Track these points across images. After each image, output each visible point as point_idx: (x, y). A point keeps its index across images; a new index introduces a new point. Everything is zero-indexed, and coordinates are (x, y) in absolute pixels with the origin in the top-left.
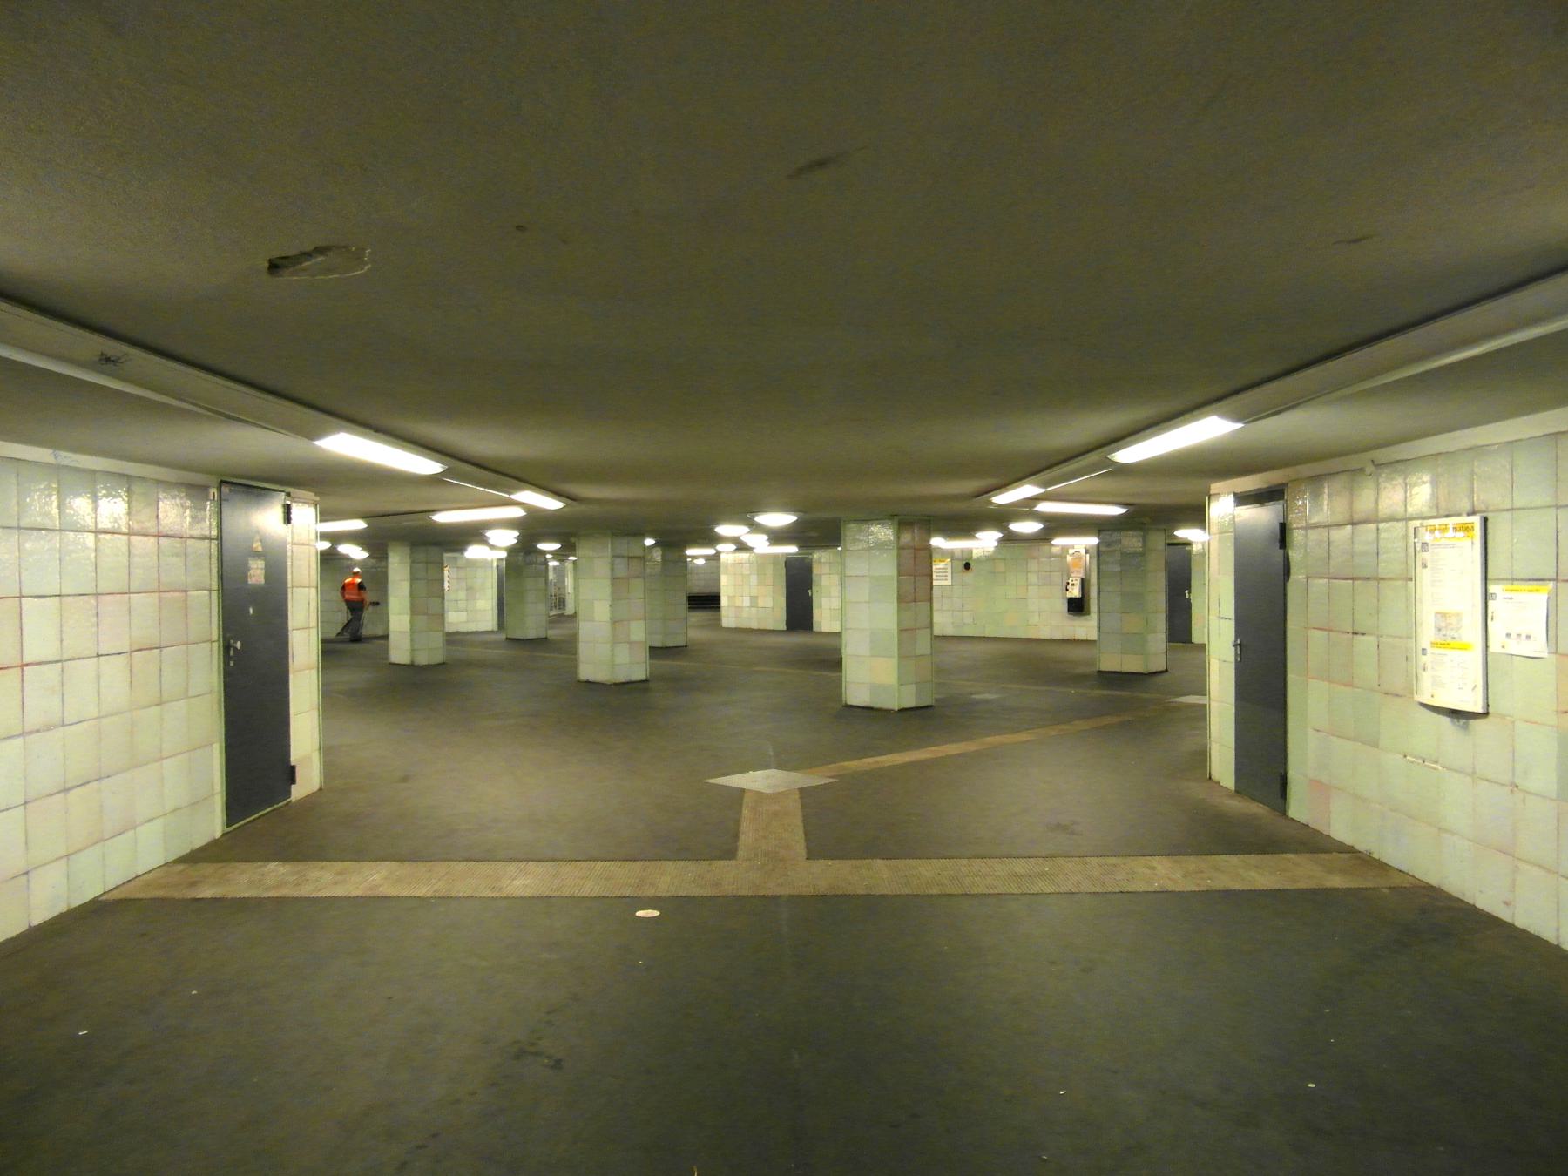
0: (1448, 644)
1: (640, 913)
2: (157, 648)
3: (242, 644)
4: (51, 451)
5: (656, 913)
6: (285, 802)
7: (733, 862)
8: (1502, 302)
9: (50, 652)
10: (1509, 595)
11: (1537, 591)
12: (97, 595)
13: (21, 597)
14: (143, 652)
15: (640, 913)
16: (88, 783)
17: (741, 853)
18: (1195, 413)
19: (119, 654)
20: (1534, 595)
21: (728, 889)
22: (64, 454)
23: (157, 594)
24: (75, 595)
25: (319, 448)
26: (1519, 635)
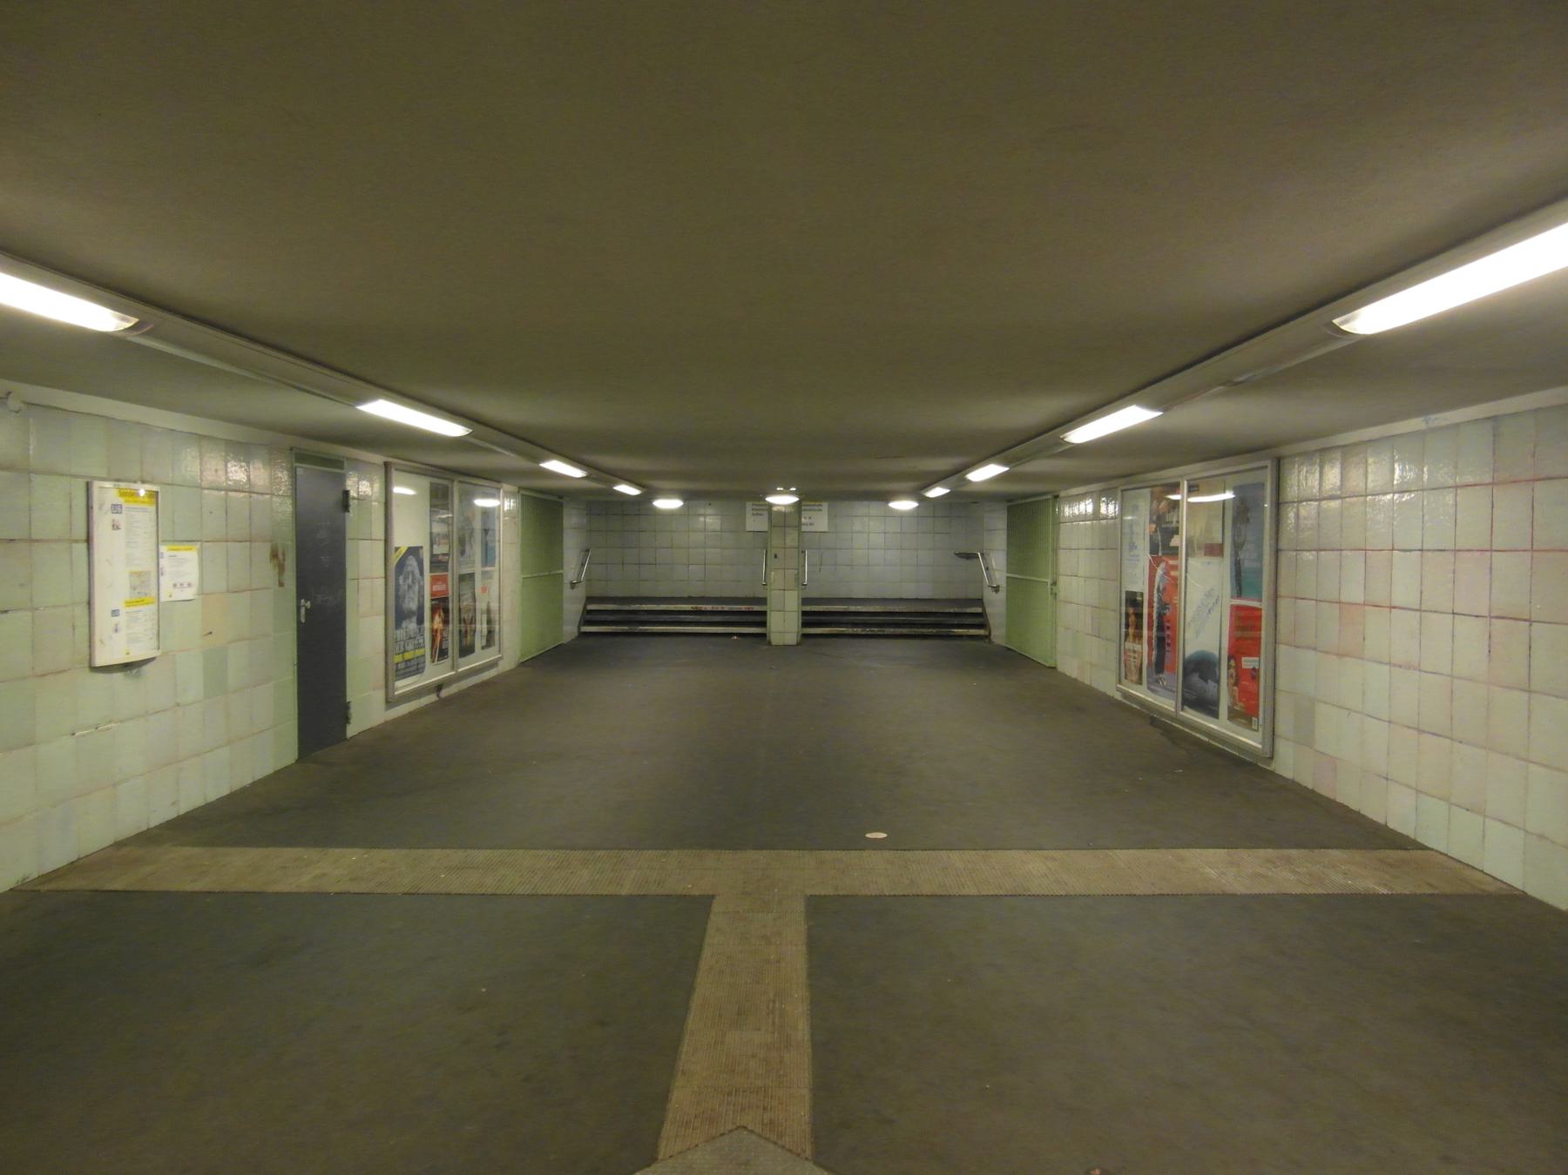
0: (143, 601)
1: (882, 835)
2: (1525, 620)
3: (670, 514)
4: (1422, 418)
5: (868, 835)
6: (1125, 701)
7: (809, 892)
8: (530, 446)
9: (1413, 601)
10: (174, 553)
11: (190, 549)
12: (1491, 550)
13: (1393, 550)
14: (1508, 621)
15: (882, 835)
16: (1440, 736)
17: (800, 907)
18: (457, 418)
19: (1477, 616)
20: (189, 552)
21: (808, 859)
22: (1433, 417)
23: (1530, 553)
24: (1434, 550)
25: (542, 468)
26: (181, 585)
